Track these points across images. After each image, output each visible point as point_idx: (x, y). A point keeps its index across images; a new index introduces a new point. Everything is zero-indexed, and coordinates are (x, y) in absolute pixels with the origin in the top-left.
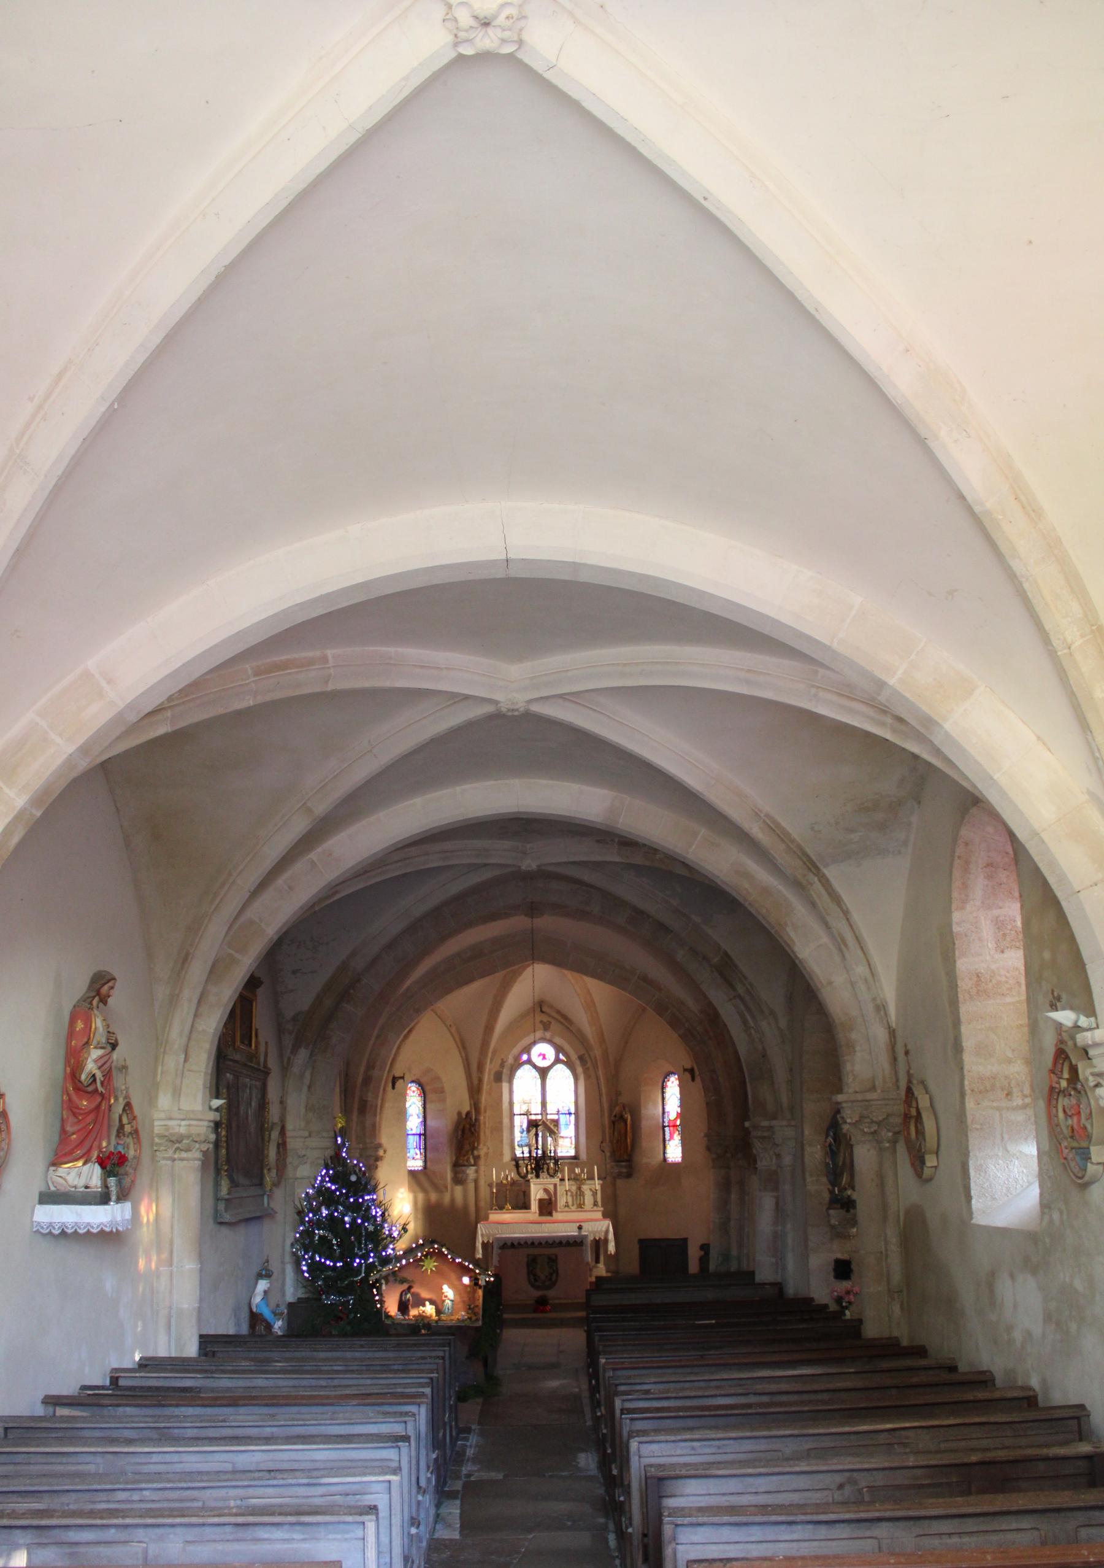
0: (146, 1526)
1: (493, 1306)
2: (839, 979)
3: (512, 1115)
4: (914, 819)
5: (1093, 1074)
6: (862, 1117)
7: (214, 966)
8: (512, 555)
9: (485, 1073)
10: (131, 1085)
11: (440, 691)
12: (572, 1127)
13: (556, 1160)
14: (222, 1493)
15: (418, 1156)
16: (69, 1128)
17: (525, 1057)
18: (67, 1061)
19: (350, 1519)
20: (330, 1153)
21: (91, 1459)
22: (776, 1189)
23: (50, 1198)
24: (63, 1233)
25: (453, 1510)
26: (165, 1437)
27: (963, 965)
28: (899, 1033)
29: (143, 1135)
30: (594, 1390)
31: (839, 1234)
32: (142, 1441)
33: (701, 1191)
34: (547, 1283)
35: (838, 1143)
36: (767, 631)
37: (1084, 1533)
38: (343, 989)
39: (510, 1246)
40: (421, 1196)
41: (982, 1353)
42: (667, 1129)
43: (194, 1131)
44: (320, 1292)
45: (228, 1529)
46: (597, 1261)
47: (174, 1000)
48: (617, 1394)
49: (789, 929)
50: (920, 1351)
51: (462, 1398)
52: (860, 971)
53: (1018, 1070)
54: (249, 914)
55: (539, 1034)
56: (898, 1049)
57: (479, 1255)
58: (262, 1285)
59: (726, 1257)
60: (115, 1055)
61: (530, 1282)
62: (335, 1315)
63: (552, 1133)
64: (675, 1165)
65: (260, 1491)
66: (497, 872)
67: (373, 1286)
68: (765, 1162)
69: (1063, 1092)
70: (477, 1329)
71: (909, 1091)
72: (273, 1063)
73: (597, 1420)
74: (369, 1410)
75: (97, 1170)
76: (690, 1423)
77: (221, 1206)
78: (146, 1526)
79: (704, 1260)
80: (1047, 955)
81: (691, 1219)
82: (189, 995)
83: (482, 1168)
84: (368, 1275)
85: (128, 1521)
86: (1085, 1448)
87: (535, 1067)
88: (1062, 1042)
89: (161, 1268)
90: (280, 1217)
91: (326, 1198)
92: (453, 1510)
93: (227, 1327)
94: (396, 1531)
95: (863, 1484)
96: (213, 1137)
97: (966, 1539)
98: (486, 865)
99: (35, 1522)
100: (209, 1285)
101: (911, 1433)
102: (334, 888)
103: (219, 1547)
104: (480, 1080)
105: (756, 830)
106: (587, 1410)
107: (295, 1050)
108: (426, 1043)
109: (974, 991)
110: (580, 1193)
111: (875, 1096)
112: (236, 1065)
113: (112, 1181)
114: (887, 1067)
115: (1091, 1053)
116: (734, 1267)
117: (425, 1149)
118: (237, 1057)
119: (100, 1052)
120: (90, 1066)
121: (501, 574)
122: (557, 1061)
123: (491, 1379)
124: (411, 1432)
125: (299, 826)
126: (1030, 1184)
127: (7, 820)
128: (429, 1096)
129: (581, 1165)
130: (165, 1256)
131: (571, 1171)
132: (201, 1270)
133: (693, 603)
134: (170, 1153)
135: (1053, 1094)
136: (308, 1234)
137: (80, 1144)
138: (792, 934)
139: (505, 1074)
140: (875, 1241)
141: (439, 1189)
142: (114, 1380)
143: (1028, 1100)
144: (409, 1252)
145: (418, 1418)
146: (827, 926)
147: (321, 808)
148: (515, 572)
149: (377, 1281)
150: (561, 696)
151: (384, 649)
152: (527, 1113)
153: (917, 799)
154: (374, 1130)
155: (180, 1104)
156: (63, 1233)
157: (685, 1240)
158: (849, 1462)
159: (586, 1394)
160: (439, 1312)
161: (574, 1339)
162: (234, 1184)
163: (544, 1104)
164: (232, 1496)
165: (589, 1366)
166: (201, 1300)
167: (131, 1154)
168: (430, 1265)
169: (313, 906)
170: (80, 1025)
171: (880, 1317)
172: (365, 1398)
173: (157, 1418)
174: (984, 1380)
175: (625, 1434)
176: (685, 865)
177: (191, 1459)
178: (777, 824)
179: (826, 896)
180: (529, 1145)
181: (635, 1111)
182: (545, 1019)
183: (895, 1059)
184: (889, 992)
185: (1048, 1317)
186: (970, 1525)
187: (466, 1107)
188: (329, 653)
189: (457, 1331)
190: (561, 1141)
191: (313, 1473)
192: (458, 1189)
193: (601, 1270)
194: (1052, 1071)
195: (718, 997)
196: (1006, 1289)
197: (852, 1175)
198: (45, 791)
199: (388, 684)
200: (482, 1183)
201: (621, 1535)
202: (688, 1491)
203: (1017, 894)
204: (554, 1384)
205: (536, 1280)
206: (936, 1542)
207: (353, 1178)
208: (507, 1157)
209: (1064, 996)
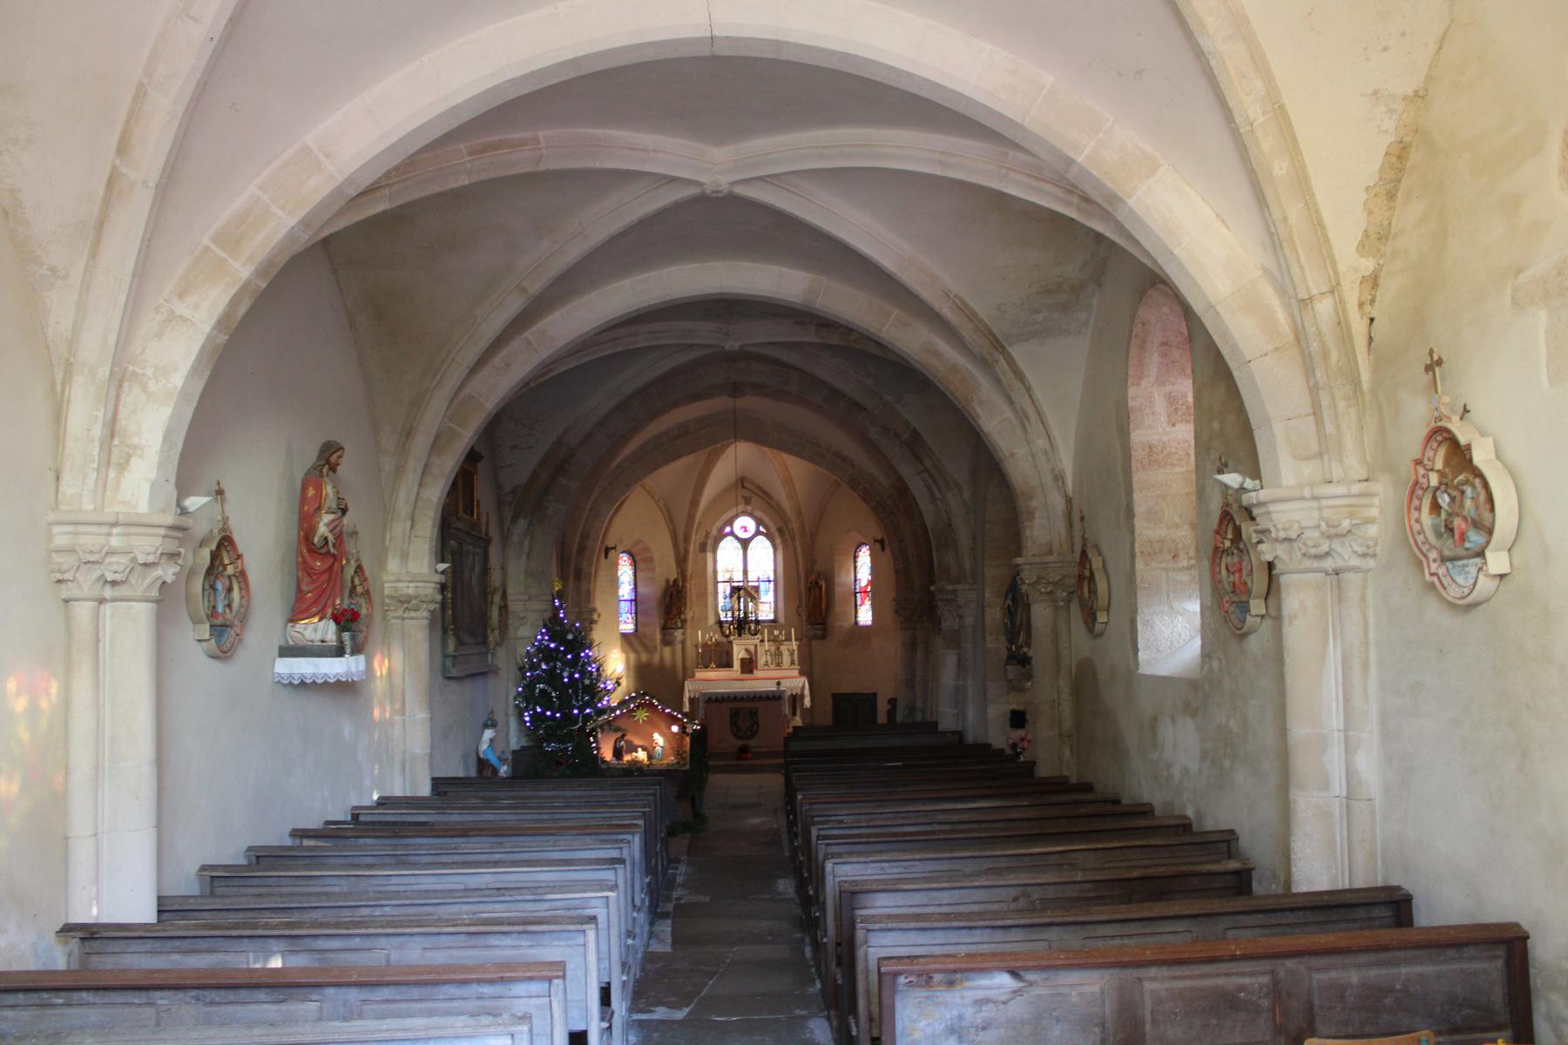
0: (388, 935)
1: (700, 753)
2: (1021, 451)
3: (716, 583)
4: (1095, 301)
5: (1256, 532)
6: (1039, 578)
7: (437, 437)
8: (716, 33)
9: (691, 543)
10: (361, 549)
11: (649, 174)
12: (771, 594)
13: (757, 622)
14: (456, 908)
16: (305, 588)
17: (728, 529)
18: (301, 527)
19: (572, 927)
20: (548, 615)
21: (335, 881)
23: (288, 651)
24: (303, 684)
25: (665, 928)
26: (401, 862)
27: (1138, 437)
28: (1075, 502)
29: (375, 597)
30: (791, 824)
31: (1015, 687)
32: (382, 866)
33: (891, 649)
35: (1016, 601)
36: (961, 109)
37: (1230, 933)
38: (557, 465)
39: (714, 700)
40: (632, 656)
41: (1142, 787)
43: (421, 592)
44: (540, 741)
45: (462, 937)
46: (794, 714)
47: (399, 470)
48: (814, 824)
49: (975, 405)
50: (1087, 788)
51: (672, 833)
52: (1040, 443)
53: (1184, 534)
54: (468, 390)
55: (741, 508)
56: (1074, 515)
57: (687, 709)
58: (488, 734)
59: (912, 710)
60: (345, 520)
62: (555, 761)
63: (753, 599)
64: (866, 627)
65: (490, 907)
66: (701, 352)
67: (590, 734)
68: (949, 622)
69: (1226, 551)
70: (685, 772)
71: (1084, 554)
72: (494, 532)
73: (794, 850)
74: (589, 839)
75: (332, 626)
76: (880, 847)
77: (449, 662)
78: (388, 935)
79: (891, 713)
80: (1216, 426)
81: (880, 676)
82: (413, 466)
83: (689, 631)
84: (585, 724)
85: (371, 931)
86: (1234, 865)
87: (737, 538)
88: (1227, 505)
89: (395, 717)
90: (503, 673)
91: (546, 654)
92: (665, 928)
93: (455, 769)
94: (614, 939)
95: (1036, 896)
96: (439, 597)
97: (1126, 941)
98: (691, 345)
99: (287, 932)
100: (440, 733)
101: (1079, 855)
102: (546, 366)
103: (454, 952)
104: (687, 551)
105: (946, 311)
106: (785, 843)
107: (514, 519)
108: (636, 515)
109: (1146, 462)
110: (779, 653)
111: (1051, 559)
112: (459, 533)
113: (346, 636)
114: (1063, 532)
115: (1255, 512)
116: (919, 717)
118: (460, 525)
119: (331, 517)
120: (322, 529)
121: (706, 52)
122: (758, 533)
123: (699, 817)
124: (626, 855)
125: (515, 305)
126: (1192, 638)
127: (233, 291)
128: (640, 565)
129: (780, 628)
130: (398, 706)
131: (770, 633)
132: (431, 719)
133: (890, 80)
134: (400, 612)
135: (1217, 553)
136: (529, 687)
137: (315, 603)
138: (978, 410)
139: (710, 544)
140: (1049, 691)
141: (650, 650)
142: (355, 817)
143: (1193, 562)
144: (623, 703)
145: (634, 846)
146: (1011, 402)
147: (535, 288)
148: (720, 50)
149: (593, 730)
150: (761, 179)
151: (591, 131)
152: (730, 581)
153: (1101, 275)
154: (589, 596)
155: (408, 567)
156: (303, 684)
157: (875, 694)
158: (1023, 878)
159: (784, 829)
160: (650, 757)
161: (773, 783)
162: (460, 643)
163: (745, 572)
164: (465, 911)
165: (787, 803)
166: (432, 747)
167: (363, 612)
168: (642, 715)
169: (528, 383)
170: (311, 492)
171: (1050, 755)
172: (584, 830)
173: (395, 847)
174: (1145, 810)
175: (821, 858)
176: (879, 344)
177: (427, 880)
178: (964, 303)
179: (1011, 375)
180: (732, 609)
181: (829, 578)
182: (747, 494)
183: (1071, 526)
184: (1067, 463)
185: (1204, 755)
186: (1132, 928)
187: (673, 575)
188: (541, 134)
189: (666, 774)
190: (761, 607)
191: (537, 890)
192: (667, 651)
193: (798, 721)
194: (1217, 532)
195: (906, 470)
196: (1167, 732)
197: (1029, 634)
198: (270, 262)
199: (598, 165)
200: (689, 644)
201: (817, 946)
202: (878, 903)
203: (1189, 371)
204: (756, 821)
206: (1100, 943)
207: (570, 637)
208: (711, 621)
209: (1231, 463)
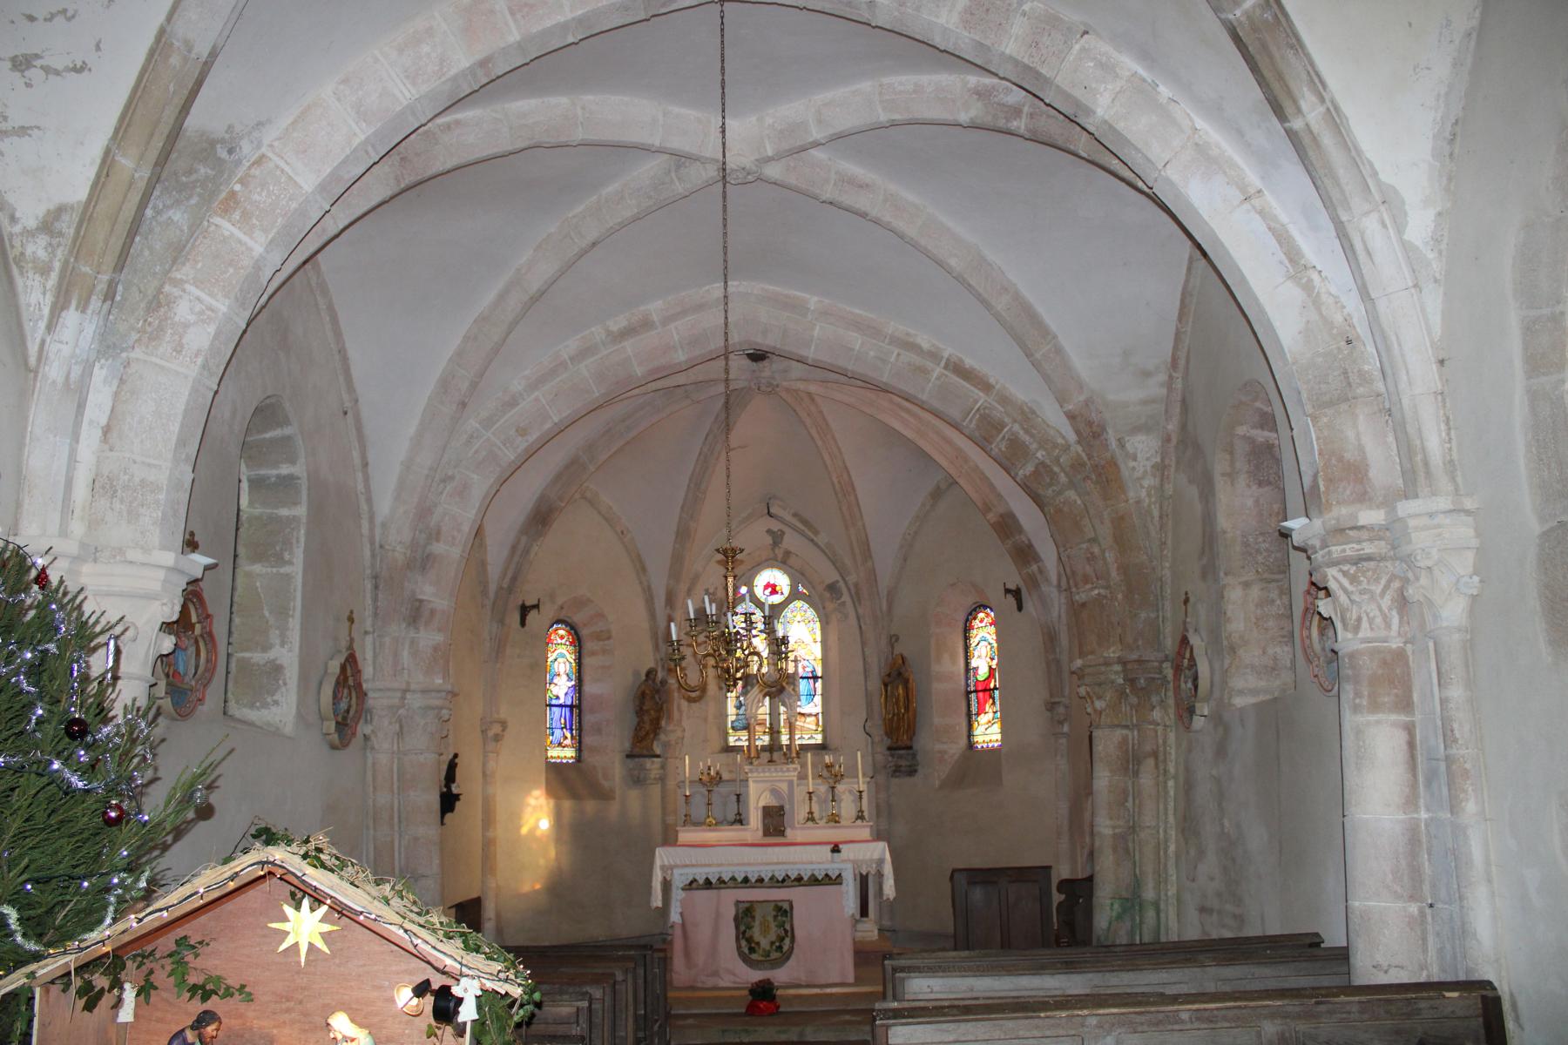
15: (568, 742)
22: (1405, 704)
34: (774, 955)
42: (973, 696)
51: (1262, 534)
59: (1132, 902)
64: (991, 753)
117: (580, 729)
122: (795, 595)
128: (589, 645)
182: (776, 526)
192: (634, 795)
205: (752, 950)
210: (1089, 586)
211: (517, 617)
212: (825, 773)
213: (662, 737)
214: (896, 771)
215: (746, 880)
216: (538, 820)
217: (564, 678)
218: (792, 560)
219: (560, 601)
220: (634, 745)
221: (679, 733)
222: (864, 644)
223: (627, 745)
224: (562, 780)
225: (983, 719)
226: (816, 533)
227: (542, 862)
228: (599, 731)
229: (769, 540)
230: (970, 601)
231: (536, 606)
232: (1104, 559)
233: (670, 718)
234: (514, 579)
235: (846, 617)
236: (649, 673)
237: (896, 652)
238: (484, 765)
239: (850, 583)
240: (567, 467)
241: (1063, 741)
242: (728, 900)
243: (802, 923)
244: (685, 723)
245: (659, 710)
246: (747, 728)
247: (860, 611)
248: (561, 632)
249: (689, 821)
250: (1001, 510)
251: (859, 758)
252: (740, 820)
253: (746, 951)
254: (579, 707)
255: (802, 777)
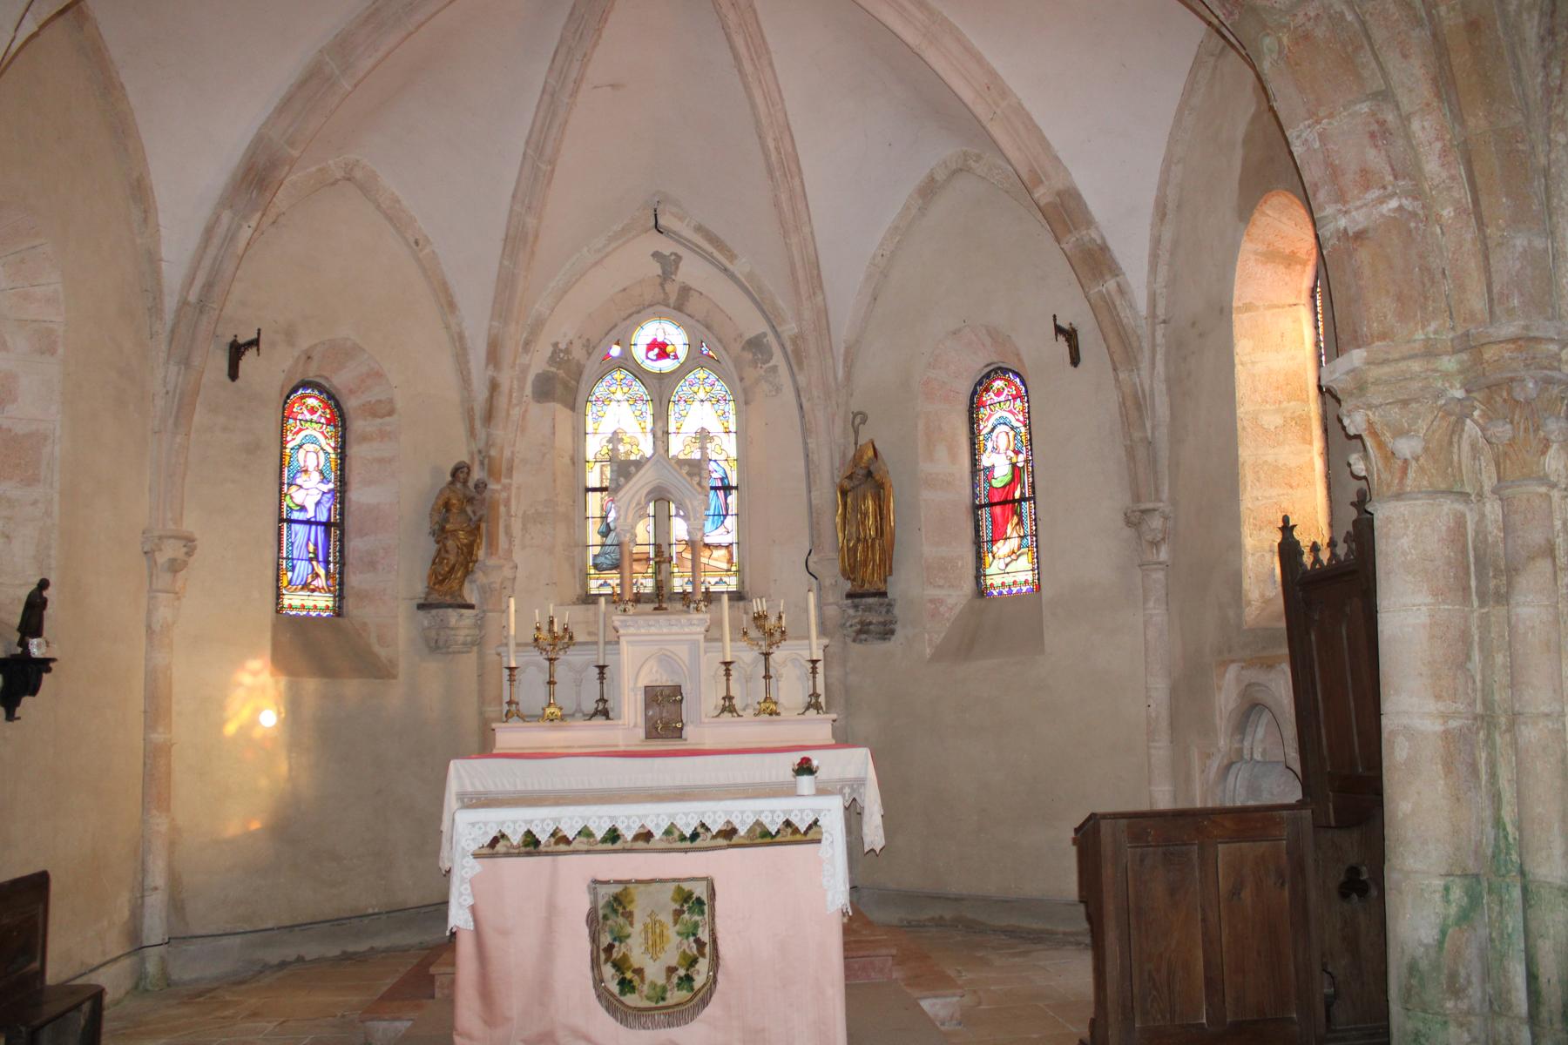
15: (321, 582)
42: (985, 513)
61: (602, 994)
64: (1013, 598)
87: (639, 374)
122: (696, 359)
128: (358, 425)
182: (666, 246)
210: (1374, 193)
211: (223, 363)
212: (754, 633)
213: (479, 576)
214: (863, 631)
215: (613, 835)
216: (258, 711)
217: (316, 477)
218: (693, 305)
219: (304, 343)
220: (431, 589)
221: (507, 572)
222: (806, 431)
223: (420, 588)
224: (308, 647)
225: (1002, 548)
226: (732, 257)
227: (263, 783)
228: (372, 565)
229: (657, 269)
230: (977, 364)
231: (254, 343)
232: (1408, 137)
233: (492, 545)
234: (209, 286)
235: (778, 390)
236: (455, 472)
237: (862, 440)
238: (150, 612)
239: (785, 336)
240: (302, 84)
241: (1159, 575)
242: (574, 882)
243: (740, 926)
244: (518, 556)
245: (475, 531)
246: (616, 566)
247: (802, 380)
248: (312, 402)
249: (513, 712)
250: (1059, 185)
251: (803, 600)
252: (603, 711)
253: (615, 989)
254: (340, 525)
255: (712, 635)
